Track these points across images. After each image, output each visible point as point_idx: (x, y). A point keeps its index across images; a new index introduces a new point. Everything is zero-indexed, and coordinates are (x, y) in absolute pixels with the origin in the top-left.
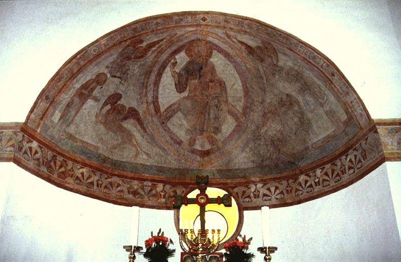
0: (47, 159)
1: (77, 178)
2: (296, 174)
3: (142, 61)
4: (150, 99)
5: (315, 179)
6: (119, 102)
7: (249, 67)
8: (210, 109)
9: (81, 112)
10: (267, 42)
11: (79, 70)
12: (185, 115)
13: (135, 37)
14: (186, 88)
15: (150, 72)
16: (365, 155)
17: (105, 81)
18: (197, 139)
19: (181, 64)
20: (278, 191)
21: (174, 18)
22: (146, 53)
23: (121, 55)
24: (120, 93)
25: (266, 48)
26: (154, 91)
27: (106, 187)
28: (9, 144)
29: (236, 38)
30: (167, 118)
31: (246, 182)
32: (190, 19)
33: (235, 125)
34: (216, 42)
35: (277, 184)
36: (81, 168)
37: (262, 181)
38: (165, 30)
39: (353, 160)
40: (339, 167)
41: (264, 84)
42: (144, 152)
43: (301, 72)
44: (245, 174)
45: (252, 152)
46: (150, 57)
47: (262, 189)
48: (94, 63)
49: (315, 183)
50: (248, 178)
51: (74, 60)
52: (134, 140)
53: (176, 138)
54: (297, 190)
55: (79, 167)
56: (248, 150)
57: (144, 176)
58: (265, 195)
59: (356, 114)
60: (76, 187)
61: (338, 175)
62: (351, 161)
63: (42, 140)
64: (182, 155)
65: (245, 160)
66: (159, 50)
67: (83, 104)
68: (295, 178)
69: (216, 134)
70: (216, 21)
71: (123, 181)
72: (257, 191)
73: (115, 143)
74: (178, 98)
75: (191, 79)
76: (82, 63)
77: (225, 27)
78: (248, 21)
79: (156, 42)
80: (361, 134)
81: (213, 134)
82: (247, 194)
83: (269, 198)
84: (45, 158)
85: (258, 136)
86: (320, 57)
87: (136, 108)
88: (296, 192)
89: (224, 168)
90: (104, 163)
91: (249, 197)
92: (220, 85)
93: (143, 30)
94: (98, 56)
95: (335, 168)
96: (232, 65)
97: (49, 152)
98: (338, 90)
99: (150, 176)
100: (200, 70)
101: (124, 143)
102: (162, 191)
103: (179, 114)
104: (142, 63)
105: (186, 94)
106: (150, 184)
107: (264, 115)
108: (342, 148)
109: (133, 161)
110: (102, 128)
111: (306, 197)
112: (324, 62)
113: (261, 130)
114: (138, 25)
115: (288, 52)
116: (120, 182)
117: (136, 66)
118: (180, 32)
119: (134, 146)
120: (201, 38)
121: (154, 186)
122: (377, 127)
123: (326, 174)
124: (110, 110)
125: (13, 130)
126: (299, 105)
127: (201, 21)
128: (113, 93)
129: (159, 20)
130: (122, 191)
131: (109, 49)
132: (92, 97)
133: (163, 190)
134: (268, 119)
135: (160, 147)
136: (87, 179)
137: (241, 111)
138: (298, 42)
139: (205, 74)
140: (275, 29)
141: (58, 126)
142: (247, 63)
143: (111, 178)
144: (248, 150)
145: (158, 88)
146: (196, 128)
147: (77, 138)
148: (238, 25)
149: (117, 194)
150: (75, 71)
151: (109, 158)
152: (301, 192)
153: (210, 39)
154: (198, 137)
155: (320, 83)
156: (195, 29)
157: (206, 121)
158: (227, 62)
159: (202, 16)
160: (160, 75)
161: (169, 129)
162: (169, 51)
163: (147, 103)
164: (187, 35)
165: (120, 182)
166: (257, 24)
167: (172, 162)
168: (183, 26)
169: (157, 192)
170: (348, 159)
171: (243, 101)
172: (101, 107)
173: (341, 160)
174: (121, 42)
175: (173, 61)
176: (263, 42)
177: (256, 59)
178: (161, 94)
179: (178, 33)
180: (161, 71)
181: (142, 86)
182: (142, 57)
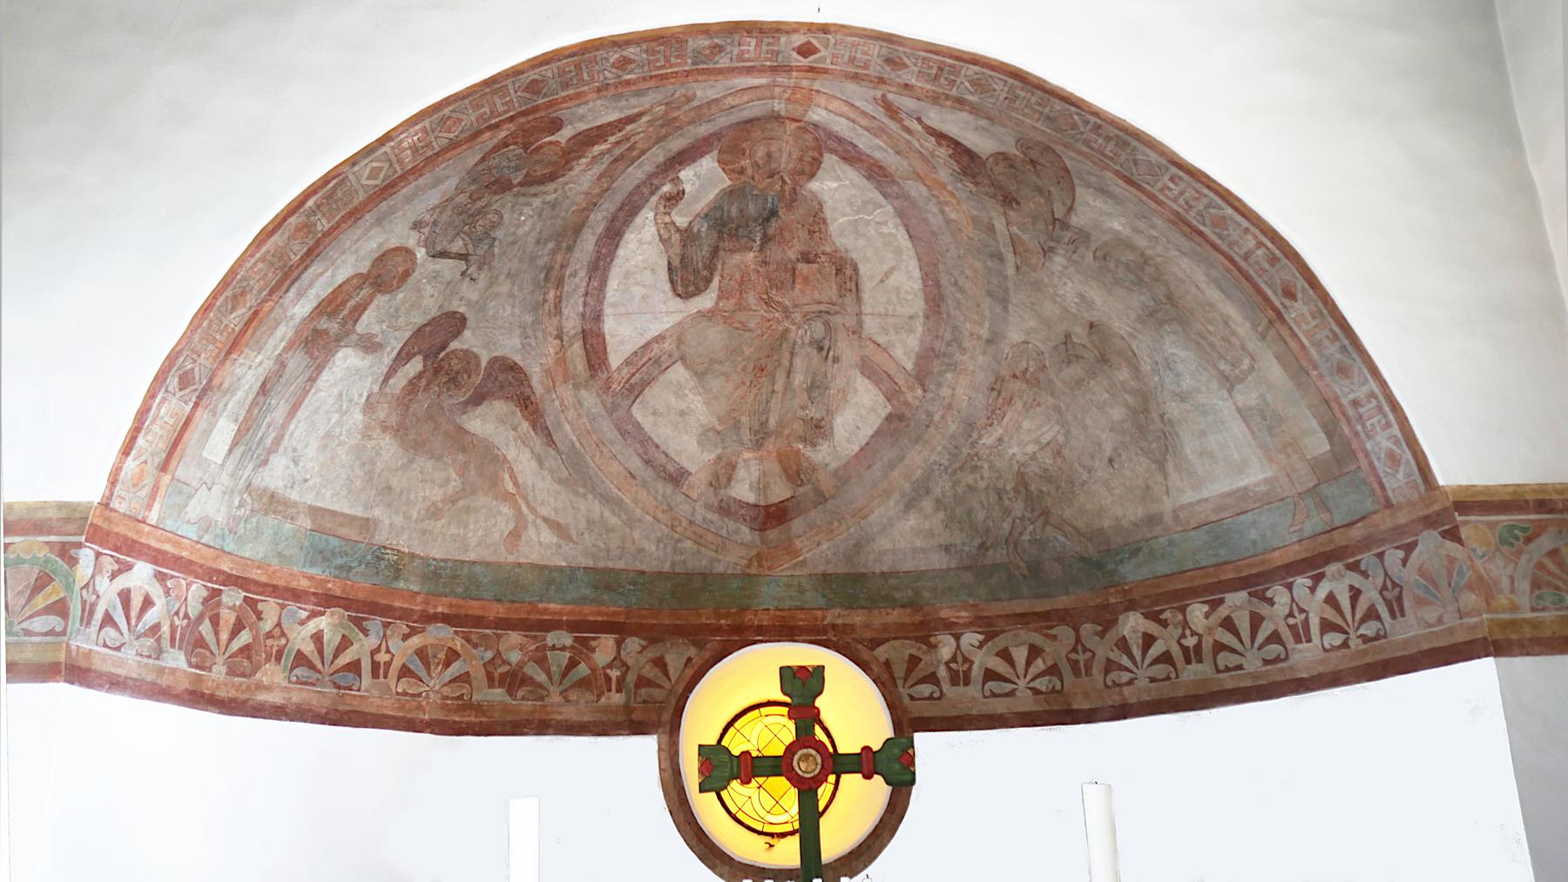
0: (186, 616)
1: (301, 659)
2: (1106, 607)
3: (551, 191)
4: (571, 320)
5: (1183, 636)
6: (454, 345)
7: (953, 216)
8: (792, 354)
9: (311, 401)
10: (1038, 143)
11: (309, 253)
12: (700, 375)
13: (536, 109)
14: (708, 281)
15: (578, 229)
16: (1399, 599)
17: (406, 274)
18: (741, 464)
19: (696, 198)
20: (1039, 665)
21: (690, 43)
22: (568, 162)
23: (473, 176)
24: (461, 310)
25: (1033, 162)
26: (586, 294)
27: (405, 672)
28: (41, 601)
29: (919, 120)
30: (630, 390)
31: (922, 623)
32: (752, 48)
33: (884, 413)
34: (841, 126)
35: (1038, 639)
36: (314, 614)
37: (972, 624)
38: (652, 83)
39: (1345, 601)
41: (1006, 278)
42: (545, 520)
43: (1159, 260)
44: (917, 593)
45: (942, 515)
46: (582, 177)
47: (980, 653)
48: (369, 218)
49: (1185, 650)
50: (926, 609)
51: (292, 220)
54: (1110, 666)
55: (304, 614)
56: (927, 504)
58: (990, 675)
59: (1369, 446)
60: (298, 696)
62: (1331, 600)
63: (167, 547)
64: (685, 523)
65: (918, 543)
66: (618, 151)
67: (320, 369)
68: (1106, 619)
69: (814, 445)
70: (852, 60)
72: (960, 659)
73: (437, 494)
74: (678, 318)
75: (732, 251)
76: (323, 225)
77: (882, 80)
78: (977, 68)
79: (609, 124)
80: (1385, 521)
83: (1008, 687)
84: (177, 613)
85: (971, 457)
86: (1245, 223)
87: (517, 359)
88: (1107, 672)
89: (841, 569)
90: (396, 578)
91: (932, 679)
92: (838, 271)
93: (565, 86)
94: (388, 189)
95: (1264, 609)
96: (890, 208)
97: (194, 587)
98: (1303, 346)
99: (569, 607)
100: (768, 220)
101: (468, 490)
102: (610, 666)
103: (678, 373)
104: (549, 198)
105: (706, 301)
106: (567, 639)
107: (995, 386)
108: (1296, 547)
109: (504, 556)
110: (388, 449)
111: (1145, 697)
112: (1260, 244)
113: (980, 437)
114: (548, 71)
115: (1119, 187)
116: (458, 644)
117: (527, 210)
118: (705, 91)
119: (507, 497)
120: (783, 113)
121: (583, 648)
122: (1459, 518)
123: (1228, 624)
124: (420, 376)
125: (53, 538)
126: (1135, 369)
127: (795, 54)
128: (434, 312)
129: (631, 52)
130: (464, 678)
131: (432, 161)
132: (354, 337)
133: (617, 661)
134: (1009, 402)
136: (336, 656)
137: (909, 366)
138: (1164, 162)
139: (786, 234)
140: (1078, 107)
141: (225, 478)
142: (947, 203)
143: (423, 630)
144: (927, 504)
146: (737, 425)
147: (295, 504)
148: (937, 77)
150: (295, 259)
151: (413, 556)
152: (1126, 677)
153: (817, 115)
154: (747, 455)
155: (1231, 310)
156: (762, 81)
158: (870, 195)
159: (799, 39)
160: (613, 235)
161: (638, 427)
162: (658, 155)
164: (730, 101)
165: (458, 644)
166: (1011, 81)
168: (720, 72)
169: (594, 670)
170: (1322, 593)
172: (385, 370)
173: (1290, 587)
174: (478, 134)
175: (667, 188)
176: (1024, 144)
177: (987, 194)
178: (614, 305)
179: (699, 93)
180: (618, 224)
181: (542, 276)
182: (552, 178)
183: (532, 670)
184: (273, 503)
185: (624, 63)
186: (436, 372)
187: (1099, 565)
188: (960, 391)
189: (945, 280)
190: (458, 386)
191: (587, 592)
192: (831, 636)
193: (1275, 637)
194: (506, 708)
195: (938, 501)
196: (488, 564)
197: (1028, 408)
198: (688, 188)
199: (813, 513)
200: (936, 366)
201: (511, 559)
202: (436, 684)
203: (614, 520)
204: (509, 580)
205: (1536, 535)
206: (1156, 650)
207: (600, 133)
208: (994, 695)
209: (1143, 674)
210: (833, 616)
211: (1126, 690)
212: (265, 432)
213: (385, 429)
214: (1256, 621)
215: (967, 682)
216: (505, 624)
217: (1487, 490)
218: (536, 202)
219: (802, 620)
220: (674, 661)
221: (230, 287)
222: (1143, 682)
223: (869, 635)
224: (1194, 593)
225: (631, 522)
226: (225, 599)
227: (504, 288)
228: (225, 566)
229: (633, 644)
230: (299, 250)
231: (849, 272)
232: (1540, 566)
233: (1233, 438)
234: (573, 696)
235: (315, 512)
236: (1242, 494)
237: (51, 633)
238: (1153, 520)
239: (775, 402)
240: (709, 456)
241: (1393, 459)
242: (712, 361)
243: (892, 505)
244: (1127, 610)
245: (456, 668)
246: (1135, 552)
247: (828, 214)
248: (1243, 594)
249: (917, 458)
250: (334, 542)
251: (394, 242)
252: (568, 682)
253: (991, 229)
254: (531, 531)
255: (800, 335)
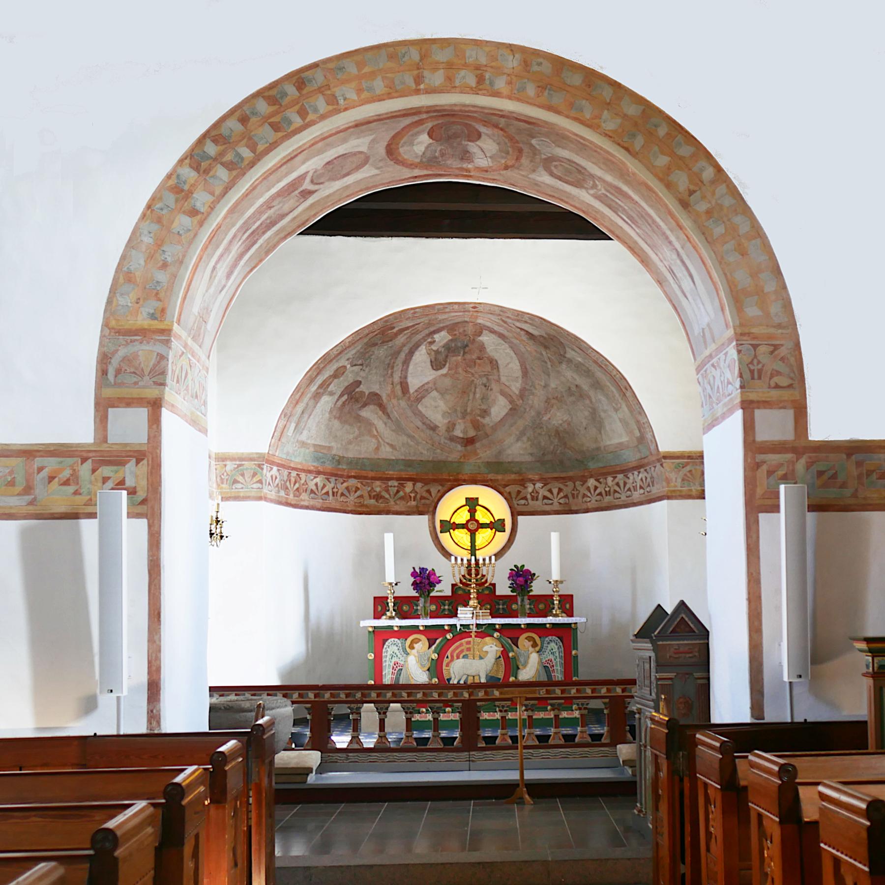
1: (312, 491)
3: (390, 344)
4: (397, 378)
6: (357, 390)
8: (475, 388)
9: (314, 413)
14: (444, 365)
19: (440, 342)
20: (562, 494)
27: (342, 494)
31: (522, 480)
34: (488, 324)
35: (562, 486)
36: (315, 477)
37: (540, 480)
40: (631, 481)
42: (388, 444)
45: (530, 443)
46: (401, 339)
48: (334, 361)
49: (606, 491)
52: (374, 430)
53: (429, 422)
54: (584, 496)
56: (525, 439)
57: (388, 474)
58: (545, 498)
60: (312, 503)
61: (629, 490)
65: (521, 452)
67: (317, 403)
68: (584, 481)
69: (484, 417)
71: (362, 483)
73: (351, 437)
74: (434, 376)
75: (453, 356)
81: (479, 418)
82: (522, 495)
83: (550, 502)
87: (378, 392)
88: (583, 498)
89: (494, 460)
90: (339, 465)
91: (525, 498)
101: (361, 434)
102: (411, 492)
105: (444, 371)
106: (396, 483)
107: (547, 401)
109: (373, 456)
110: (336, 423)
116: (359, 485)
118: (441, 317)
119: (374, 436)
123: (618, 484)
130: (361, 496)
133: (413, 491)
135: (409, 436)
137: (517, 393)
144: (525, 439)
145: (408, 367)
146: (456, 411)
149: (356, 500)
151: (343, 457)
152: (589, 499)
153: (479, 321)
154: (460, 421)
157: (471, 401)
159: (472, 305)
160: (411, 353)
161: (420, 412)
162: (427, 332)
163: (392, 384)
165: (359, 485)
167: (425, 453)
169: (405, 493)
171: (520, 382)
173: (633, 474)
175: (429, 340)
178: (411, 374)
182: (391, 340)
183: (384, 494)
184: (303, 444)
185: (415, 313)
186: (351, 399)
187: (582, 462)
188: (535, 402)
189: (528, 367)
190: (358, 402)
191: (402, 467)
192: (490, 483)
193: (629, 490)
194: (375, 506)
195: (528, 438)
196: (368, 459)
197: (558, 409)
198: (437, 340)
199: (484, 441)
200: (527, 393)
201: (376, 457)
202: (352, 498)
203: (412, 443)
204: (375, 464)
205: (686, 466)
206: (598, 491)
207: (407, 328)
208: (546, 504)
209: (594, 498)
210: (491, 476)
211: (588, 504)
212: (302, 424)
213: (335, 418)
214: (625, 484)
215: (537, 500)
216: (374, 479)
217: (674, 452)
218: (386, 347)
219: (479, 477)
220: (434, 491)
221: (298, 388)
222: (593, 501)
223: (503, 483)
224: (609, 474)
225: (418, 443)
226: (292, 474)
227: (374, 371)
228: (292, 465)
229: (419, 485)
230: (315, 374)
231: (494, 363)
232: (685, 475)
233: (618, 426)
234: (398, 502)
235: (315, 445)
236: (621, 444)
237: (259, 488)
238: (598, 449)
239: (470, 404)
240: (446, 421)
241: (651, 441)
242: (447, 390)
243: (512, 439)
244: (591, 477)
245: (358, 493)
246: (593, 459)
247: (486, 346)
248: (622, 475)
249: (521, 423)
250: (320, 454)
251: (341, 365)
252: (396, 498)
253: (542, 354)
254: (383, 447)
255: (478, 382)
